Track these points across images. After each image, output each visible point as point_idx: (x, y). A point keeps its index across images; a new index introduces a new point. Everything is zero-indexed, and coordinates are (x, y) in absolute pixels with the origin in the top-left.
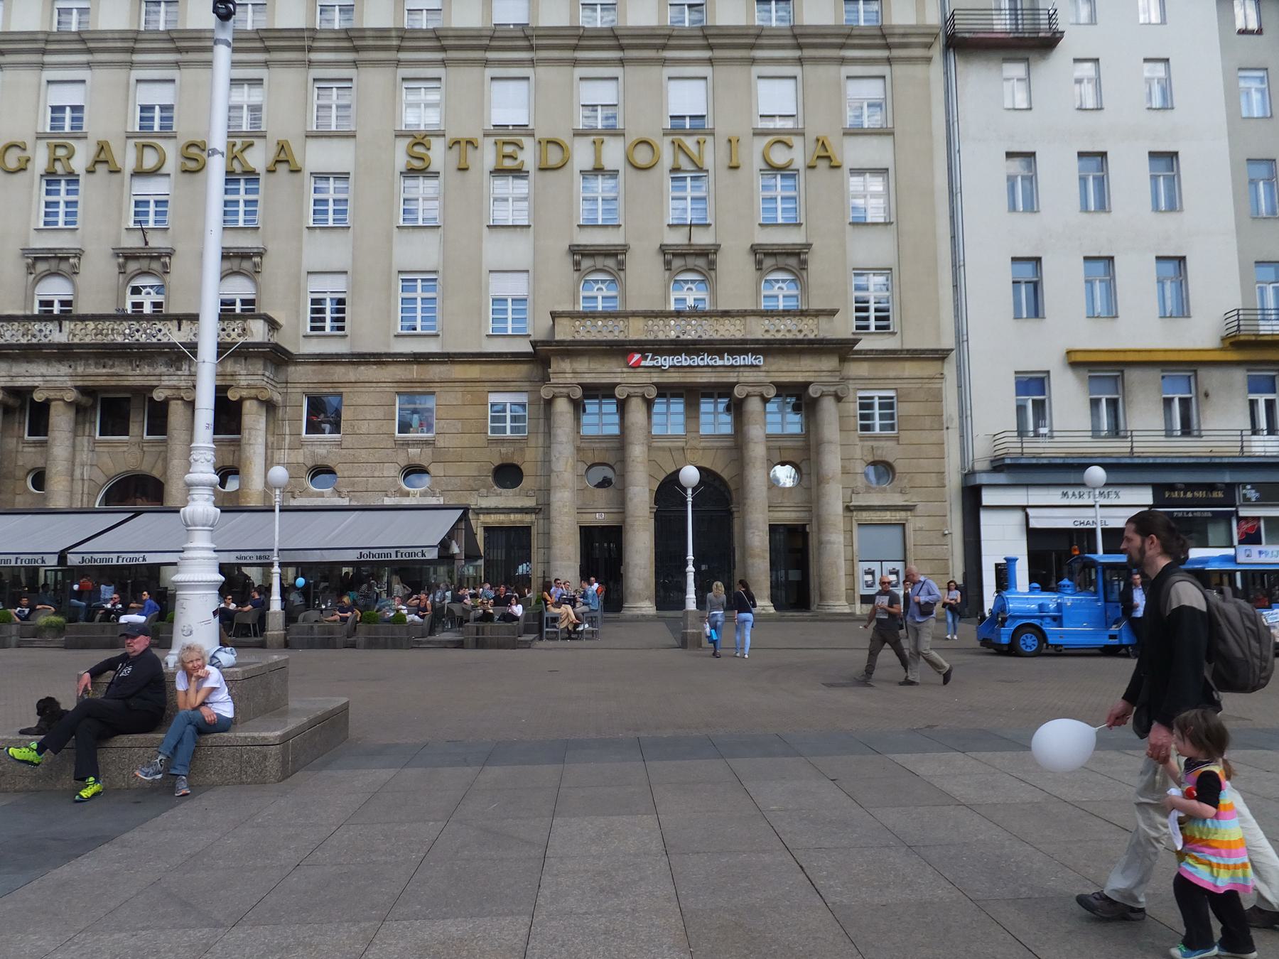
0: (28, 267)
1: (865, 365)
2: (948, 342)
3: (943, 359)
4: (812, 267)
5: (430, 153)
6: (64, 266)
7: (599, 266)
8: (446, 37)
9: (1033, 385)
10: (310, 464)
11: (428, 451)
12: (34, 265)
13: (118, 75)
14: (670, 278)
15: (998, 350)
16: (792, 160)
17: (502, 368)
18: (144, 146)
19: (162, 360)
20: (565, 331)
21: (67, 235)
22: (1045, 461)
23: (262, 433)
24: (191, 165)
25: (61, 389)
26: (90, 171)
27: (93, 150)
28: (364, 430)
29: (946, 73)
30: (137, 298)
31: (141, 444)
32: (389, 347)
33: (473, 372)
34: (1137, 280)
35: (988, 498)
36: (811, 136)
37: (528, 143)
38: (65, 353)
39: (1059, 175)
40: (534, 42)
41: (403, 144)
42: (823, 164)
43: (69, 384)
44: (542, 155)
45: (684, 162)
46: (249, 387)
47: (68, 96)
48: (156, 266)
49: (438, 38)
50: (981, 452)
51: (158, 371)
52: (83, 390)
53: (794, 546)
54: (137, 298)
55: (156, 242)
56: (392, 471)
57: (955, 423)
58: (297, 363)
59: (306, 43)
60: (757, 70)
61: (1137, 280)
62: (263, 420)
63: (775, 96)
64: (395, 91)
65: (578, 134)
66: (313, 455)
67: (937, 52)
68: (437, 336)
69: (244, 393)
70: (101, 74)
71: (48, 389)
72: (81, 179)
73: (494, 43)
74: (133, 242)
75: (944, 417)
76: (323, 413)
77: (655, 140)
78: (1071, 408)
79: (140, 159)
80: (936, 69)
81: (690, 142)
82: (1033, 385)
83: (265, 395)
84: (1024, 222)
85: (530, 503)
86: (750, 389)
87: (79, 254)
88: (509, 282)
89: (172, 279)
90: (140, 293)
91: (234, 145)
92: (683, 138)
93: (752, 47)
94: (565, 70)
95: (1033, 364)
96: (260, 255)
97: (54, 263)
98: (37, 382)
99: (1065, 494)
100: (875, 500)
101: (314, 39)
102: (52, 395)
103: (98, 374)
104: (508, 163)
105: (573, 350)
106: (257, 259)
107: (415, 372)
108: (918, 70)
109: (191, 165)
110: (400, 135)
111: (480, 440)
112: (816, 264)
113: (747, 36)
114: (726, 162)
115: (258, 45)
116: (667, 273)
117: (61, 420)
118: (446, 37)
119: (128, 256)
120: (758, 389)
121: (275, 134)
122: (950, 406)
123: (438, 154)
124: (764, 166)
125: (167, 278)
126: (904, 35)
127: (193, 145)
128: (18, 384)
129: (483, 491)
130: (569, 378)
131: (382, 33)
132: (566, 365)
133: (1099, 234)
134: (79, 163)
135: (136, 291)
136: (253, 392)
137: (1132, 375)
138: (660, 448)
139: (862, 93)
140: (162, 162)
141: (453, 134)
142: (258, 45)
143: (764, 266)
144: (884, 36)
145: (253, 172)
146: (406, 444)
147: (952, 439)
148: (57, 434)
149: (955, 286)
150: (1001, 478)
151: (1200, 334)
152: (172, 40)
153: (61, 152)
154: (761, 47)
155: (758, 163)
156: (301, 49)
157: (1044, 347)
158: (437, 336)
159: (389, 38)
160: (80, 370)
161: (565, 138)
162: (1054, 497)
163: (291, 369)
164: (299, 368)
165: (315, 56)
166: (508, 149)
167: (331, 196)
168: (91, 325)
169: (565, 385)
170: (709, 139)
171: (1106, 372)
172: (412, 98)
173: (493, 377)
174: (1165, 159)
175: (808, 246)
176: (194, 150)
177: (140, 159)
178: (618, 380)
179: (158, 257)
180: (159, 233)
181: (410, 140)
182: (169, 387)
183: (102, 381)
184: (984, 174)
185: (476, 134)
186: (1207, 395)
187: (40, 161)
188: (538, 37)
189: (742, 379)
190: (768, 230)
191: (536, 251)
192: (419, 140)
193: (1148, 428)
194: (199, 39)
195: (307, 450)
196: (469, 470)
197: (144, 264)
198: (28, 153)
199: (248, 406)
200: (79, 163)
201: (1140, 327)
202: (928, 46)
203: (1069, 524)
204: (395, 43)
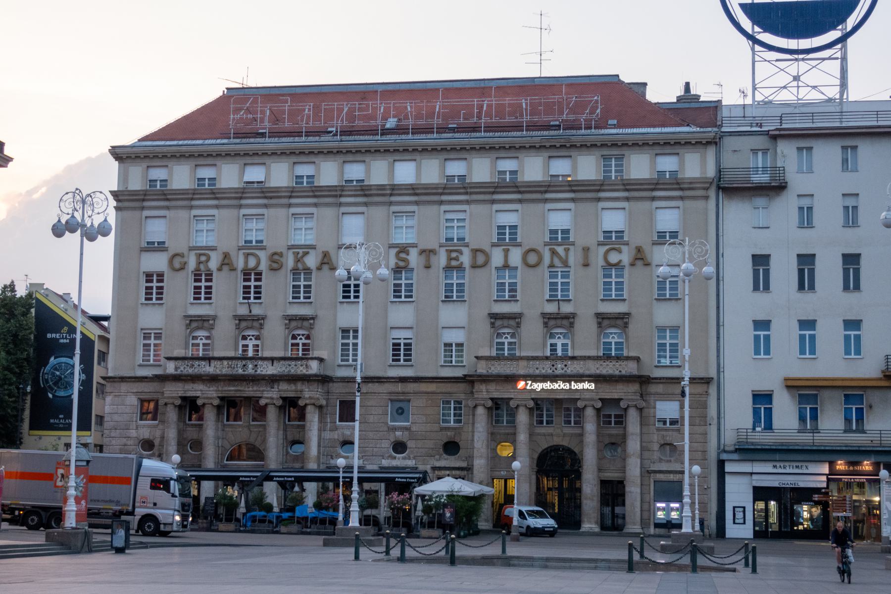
0: (187, 325)
1: (661, 386)
2: (713, 373)
3: (708, 383)
4: (630, 326)
5: (409, 257)
6: (206, 324)
7: (506, 324)
8: (418, 189)
9: (762, 399)
10: (341, 439)
11: (406, 433)
12: (190, 324)
13: (233, 212)
14: (547, 332)
15: (743, 374)
16: (620, 261)
17: (449, 385)
18: (248, 254)
19: (263, 382)
20: (482, 369)
21: (207, 307)
22: (759, 447)
23: (316, 423)
24: (275, 265)
25: (211, 398)
26: (220, 269)
27: (221, 257)
28: (371, 420)
29: (717, 205)
30: (245, 342)
31: (249, 427)
32: (385, 372)
33: (432, 387)
34: (830, 335)
35: (728, 468)
36: (633, 245)
37: (466, 251)
38: (213, 379)
39: (783, 271)
40: (469, 190)
41: (393, 252)
42: (639, 263)
43: (215, 395)
44: (474, 258)
45: (557, 262)
46: (310, 398)
47: (508, 219)
48: (256, 324)
49: (413, 189)
50: (729, 439)
51: (261, 389)
52: (222, 399)
53: (613, 492)
54: (245, 342)
55: (256, 311)
56: (387, 445)
57: (715, 421)
58: (334, 382)
59: (339, 193)
60: (496, 207)
61: (830, 335)
62: (317, 416)
63: (613, 219)
64: (388, 230)
65: (494, 245)
66: (343, 434)
67: (712, 193)
68: (412, 366)
69: (308, 402)
70: (225, 212)
71: (204, 398)
72: (214, 275)
73: (446, 191)
74: (551, 308)
75: (708, 419)
76: (347, 411)
77: (540, 248)
78: (786, 414)
79: (246, 262)
80: (712, 203)
81: (560, 250)
82: (762, 399)
83: (318, 403)
84: (761, 297)
85: (464, 465)
86: (587, 403)
87: (214, 318)
88: (454, 329)
89: (265, 332)
90: (246, 339)
91: (298, 253)
92: (555, 247)
93: (599, 191)
94: (488, 206)
95: (763, 386)
96: (313, 319)
97: (200, 323)
98: (198, 394)
99: (775, 467)
100: (664, 467)
101: (343, 190)
102: (206, 401)
103: (231, 390)
104: (454, 263)
105: (486, 379)
106: (312, 321)
107: (400, 387)
108: (700, 204)
109: (275, 265)
110: (392, 246)
111: (436, 427)
112: (634, 327)
113: (594, 185)
114: (581, 261)
115: (311, 194)
116: (545, 329)
117: (210, 415)
118: (418, 189)
119: (241, 319)
120: (592, 403)
121: (321, 248)
122: (712, 411)
123: (413, 257)
124: (603, 263)
125: (262, 331)
126: (691, 183)
127: (275, 254)
128: (188, 395)
129: (437, 457)
130: (485, 395)
131: (381, 187)
132: (483, 387)
133: (806, 305)
134: (213, 264)
135: (294, 337)
136: (313, 401)
137: (826, 394)
138: (539, 434)
139: (668, 218)
140: (258, 263)
141: (422, 246)
142: (311, 194)
143: (603, 325)
144: (678, 184)
145: (309, 269)
146: (395, 429)
147: (713, 430)
148: (209, 423)
149: (718, 338)
150: (735, 456)
151: (868, 367)
152: (263, 192)
153: (203, 258)
154: (604, 191)
155: (601, 262)
156: (336, 196)
157: (770, 378)
158: (412, 366)
159: (384, 189)
160: (220, 389)
161: (486, 248)
162: (768, 467)
163: (331, 384)
164: (335, 384)
165: (343, 200)
166: (454, 255)
167: (403, 282)
168: (225, 362)
169: (483, 399)
170: (571, 247)
171: (808, 393)
172: (398, 223)
173: (444, 390)
174: (851, 260)
175: (628, 314)
176: (276, 257)
177: (246, 262)
178: (512, 396)
179: (258, 320)
180: (257, 305)
181: (397, 249)
182: (267, 398)
183: (232, 394)
184: (738, 271)
185: (435, 246)
186: (871, 407)
187: (192, 264)
188: (471, 188)
189: (583, 397)
190: (605, 303)
191: (470, 316)
192: (403, 249)
193: (832, 424)
194: (278, 192)
195: (339, 432)
196: (430, 444)
197: (249, 324)
198: (185, 259)
199: (309, 409)
200: (213, 264)
201: (831, 363)
202: (707, 189)
203: (776, 484)
204: (388, 192)
